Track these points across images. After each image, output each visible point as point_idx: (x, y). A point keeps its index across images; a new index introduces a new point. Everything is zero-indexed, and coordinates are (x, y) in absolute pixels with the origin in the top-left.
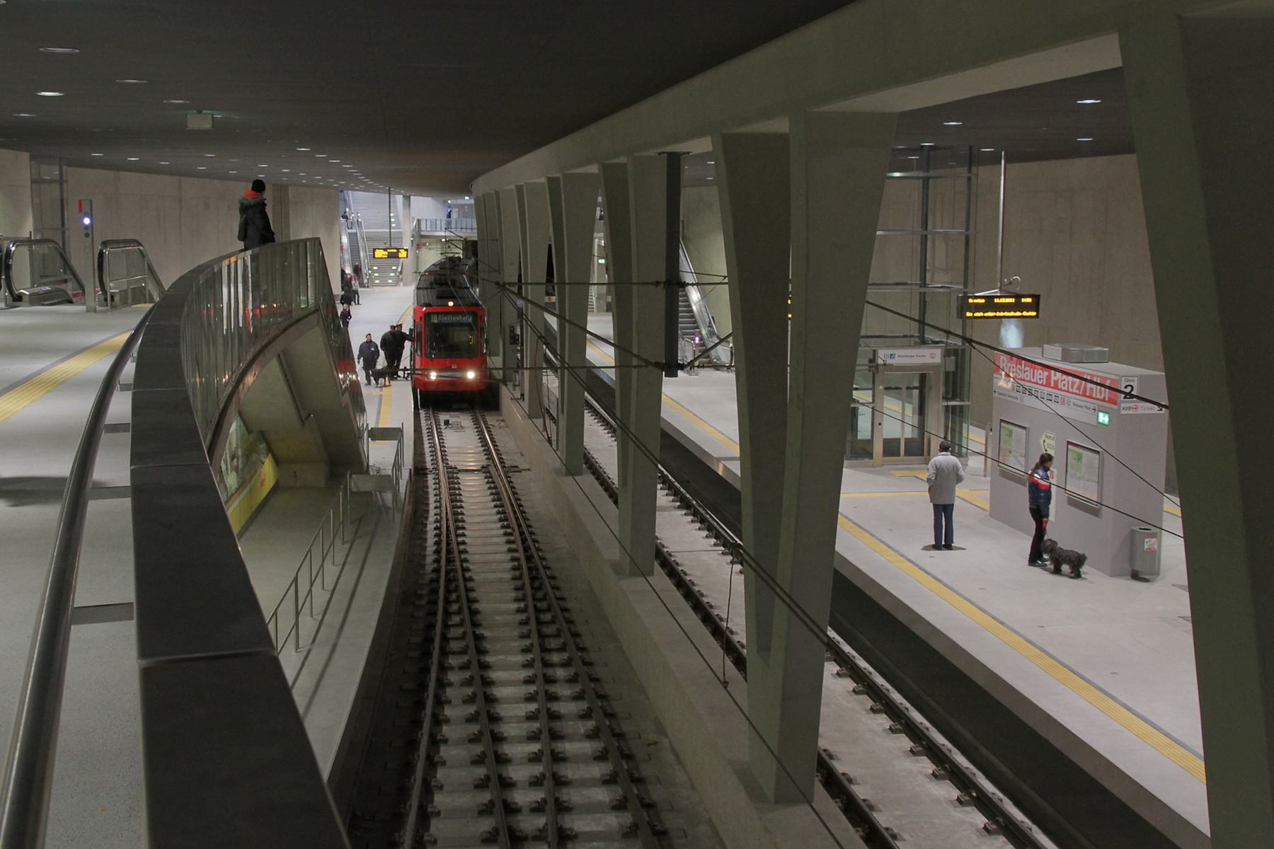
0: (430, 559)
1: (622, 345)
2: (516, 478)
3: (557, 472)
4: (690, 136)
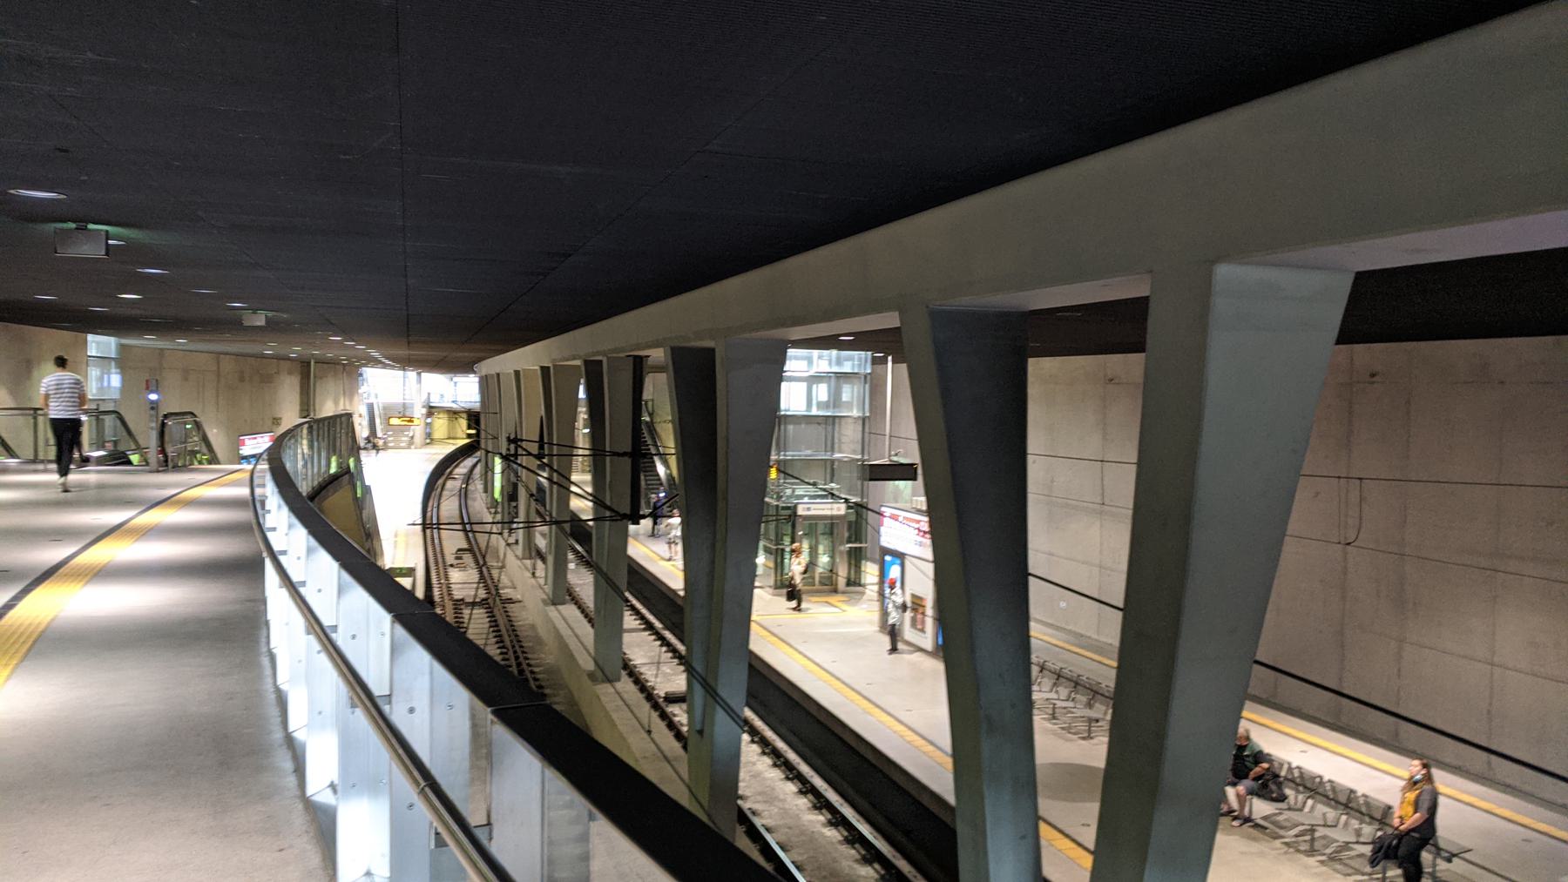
0: (630, 598)
1: (598, 501)
2: (510, 607)
3: (544, 601)
4: (649, 347)
